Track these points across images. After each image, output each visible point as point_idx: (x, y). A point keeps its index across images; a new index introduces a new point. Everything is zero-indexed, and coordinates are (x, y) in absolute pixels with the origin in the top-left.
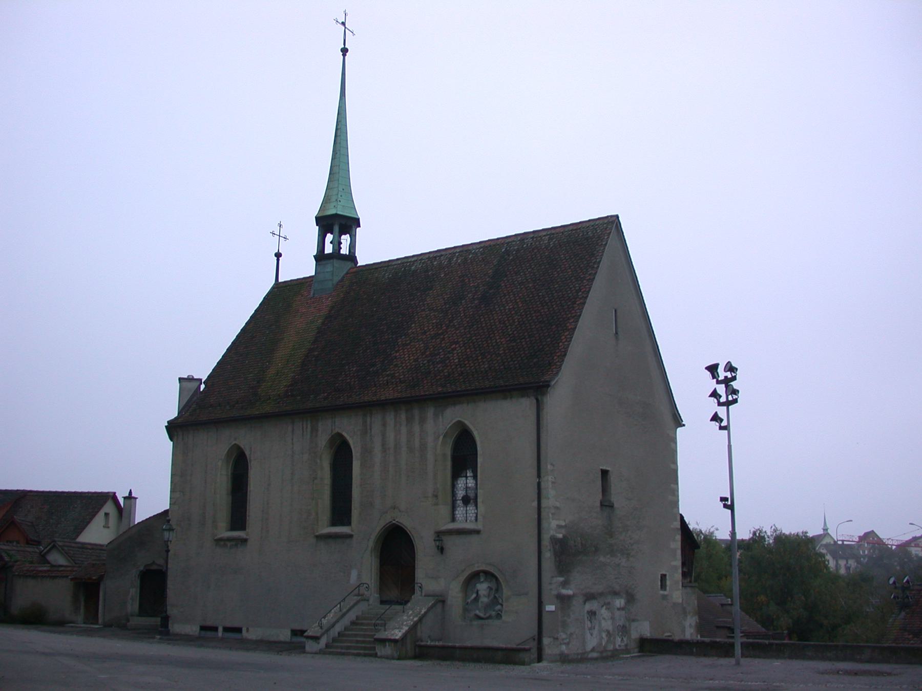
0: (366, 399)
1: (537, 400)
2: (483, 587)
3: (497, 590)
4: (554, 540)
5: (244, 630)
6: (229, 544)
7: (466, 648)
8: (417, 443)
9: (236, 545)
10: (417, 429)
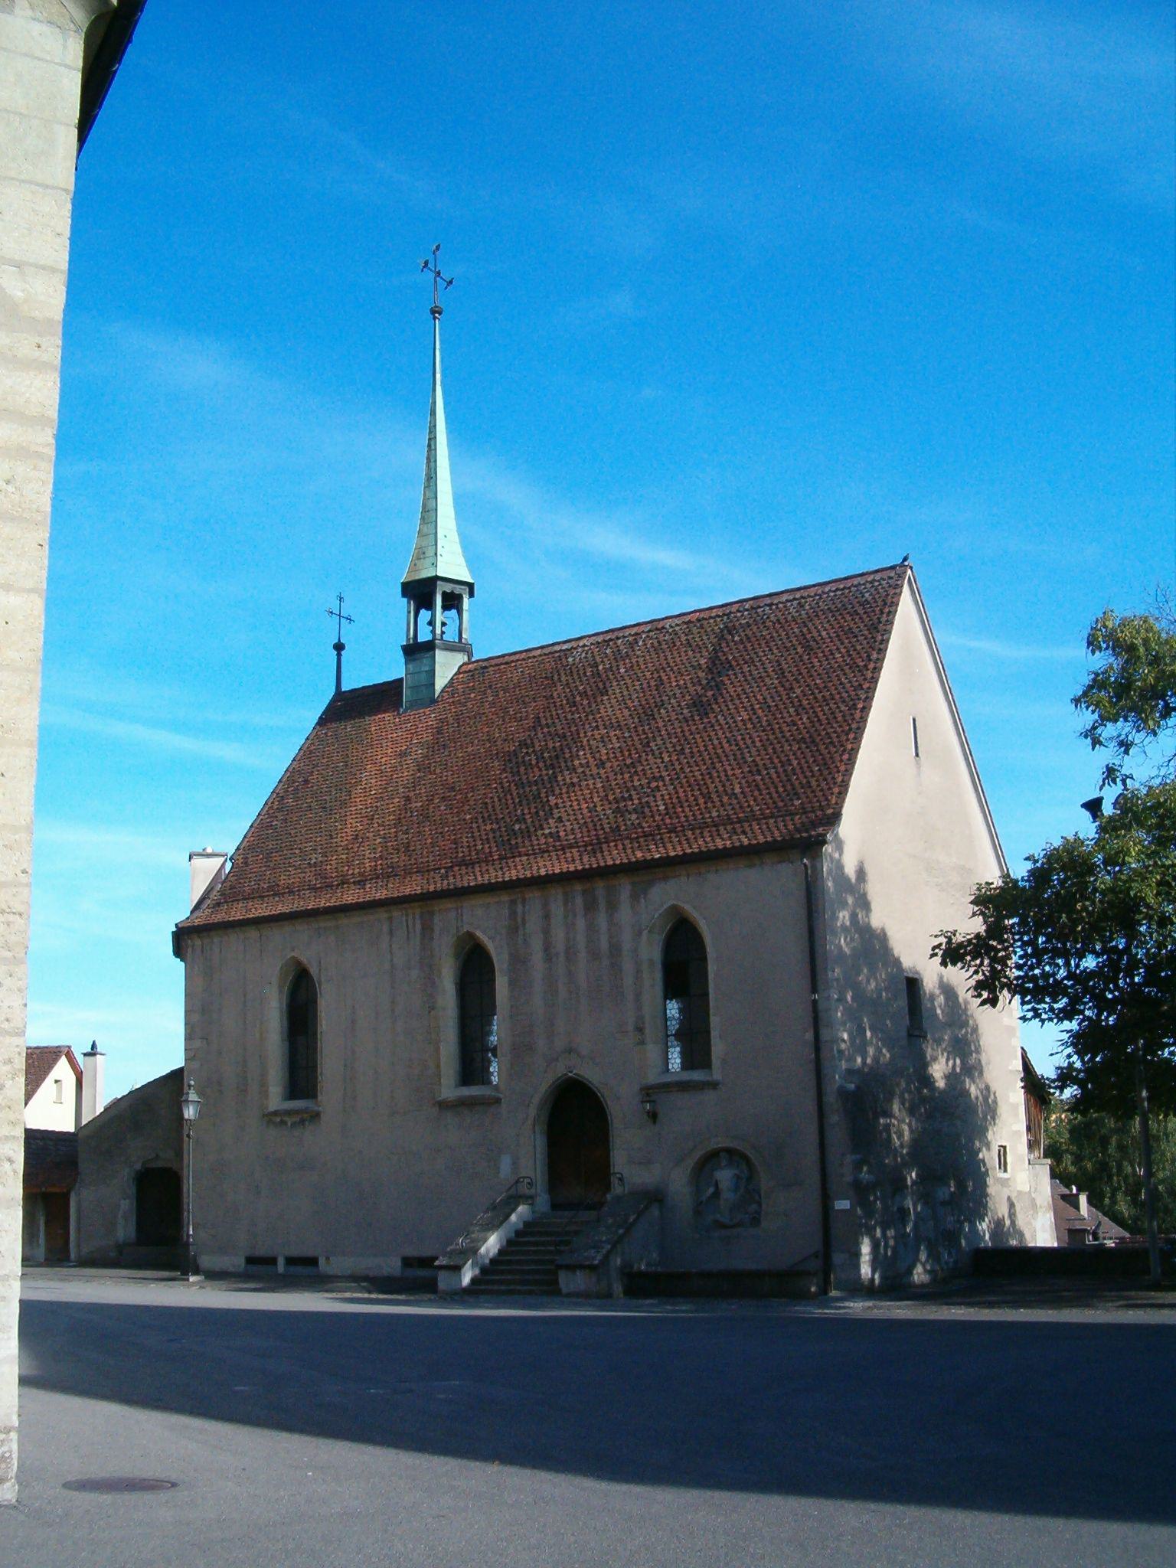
0: (408, 891)
1: (513, 914)
2: (725, 1176)
3: (750, 1179)
4: (842, 1093)
5: (322, 1261)
6: (289, 1121)
7: (709, 1275)
8: (604, 944)
9: (302, 1122)
10: (602, 920)
